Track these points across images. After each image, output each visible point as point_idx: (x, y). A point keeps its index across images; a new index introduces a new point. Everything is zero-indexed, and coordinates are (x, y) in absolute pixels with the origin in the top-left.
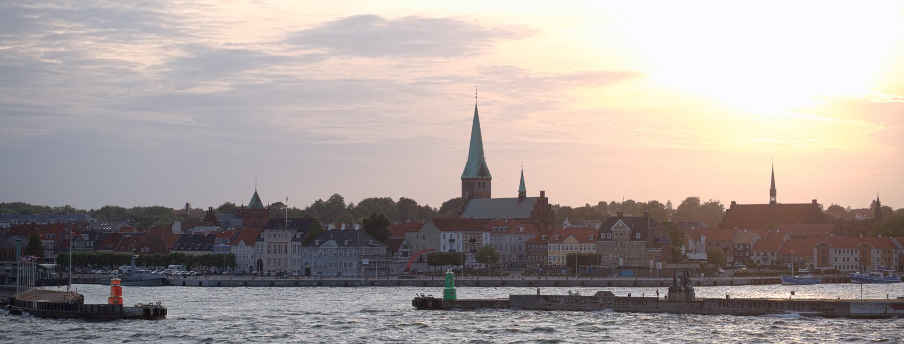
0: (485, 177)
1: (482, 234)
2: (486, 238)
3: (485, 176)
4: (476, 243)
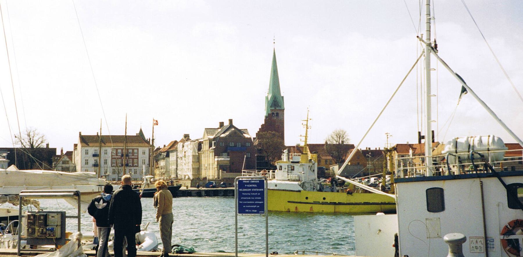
0: (278, 108)
1: (138, 149)
2: (144, 153)
3: (278, 107)
4: (131, 158)
